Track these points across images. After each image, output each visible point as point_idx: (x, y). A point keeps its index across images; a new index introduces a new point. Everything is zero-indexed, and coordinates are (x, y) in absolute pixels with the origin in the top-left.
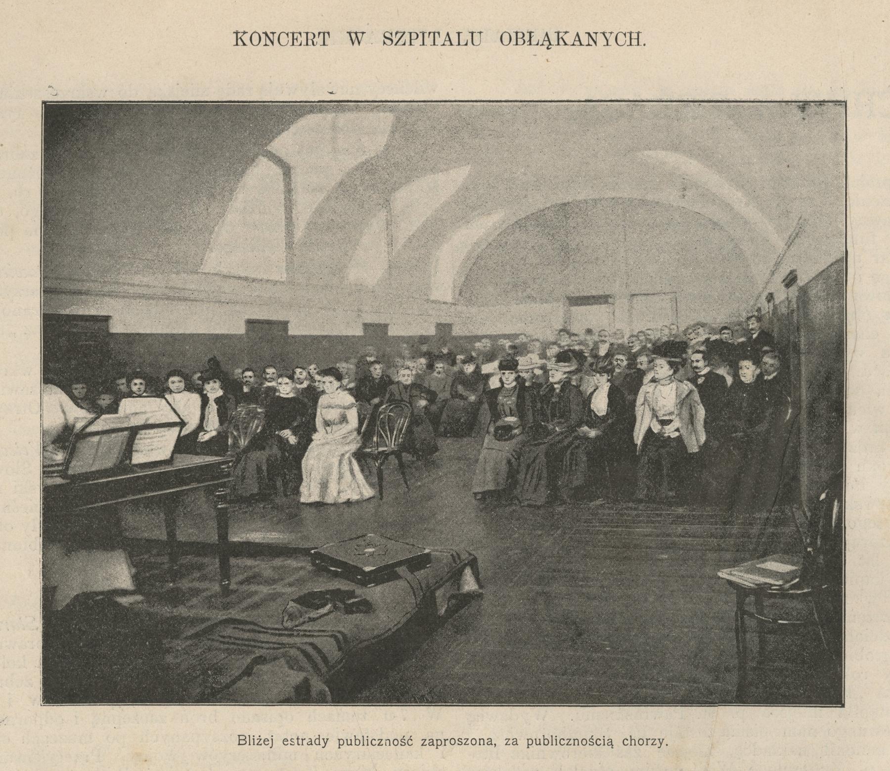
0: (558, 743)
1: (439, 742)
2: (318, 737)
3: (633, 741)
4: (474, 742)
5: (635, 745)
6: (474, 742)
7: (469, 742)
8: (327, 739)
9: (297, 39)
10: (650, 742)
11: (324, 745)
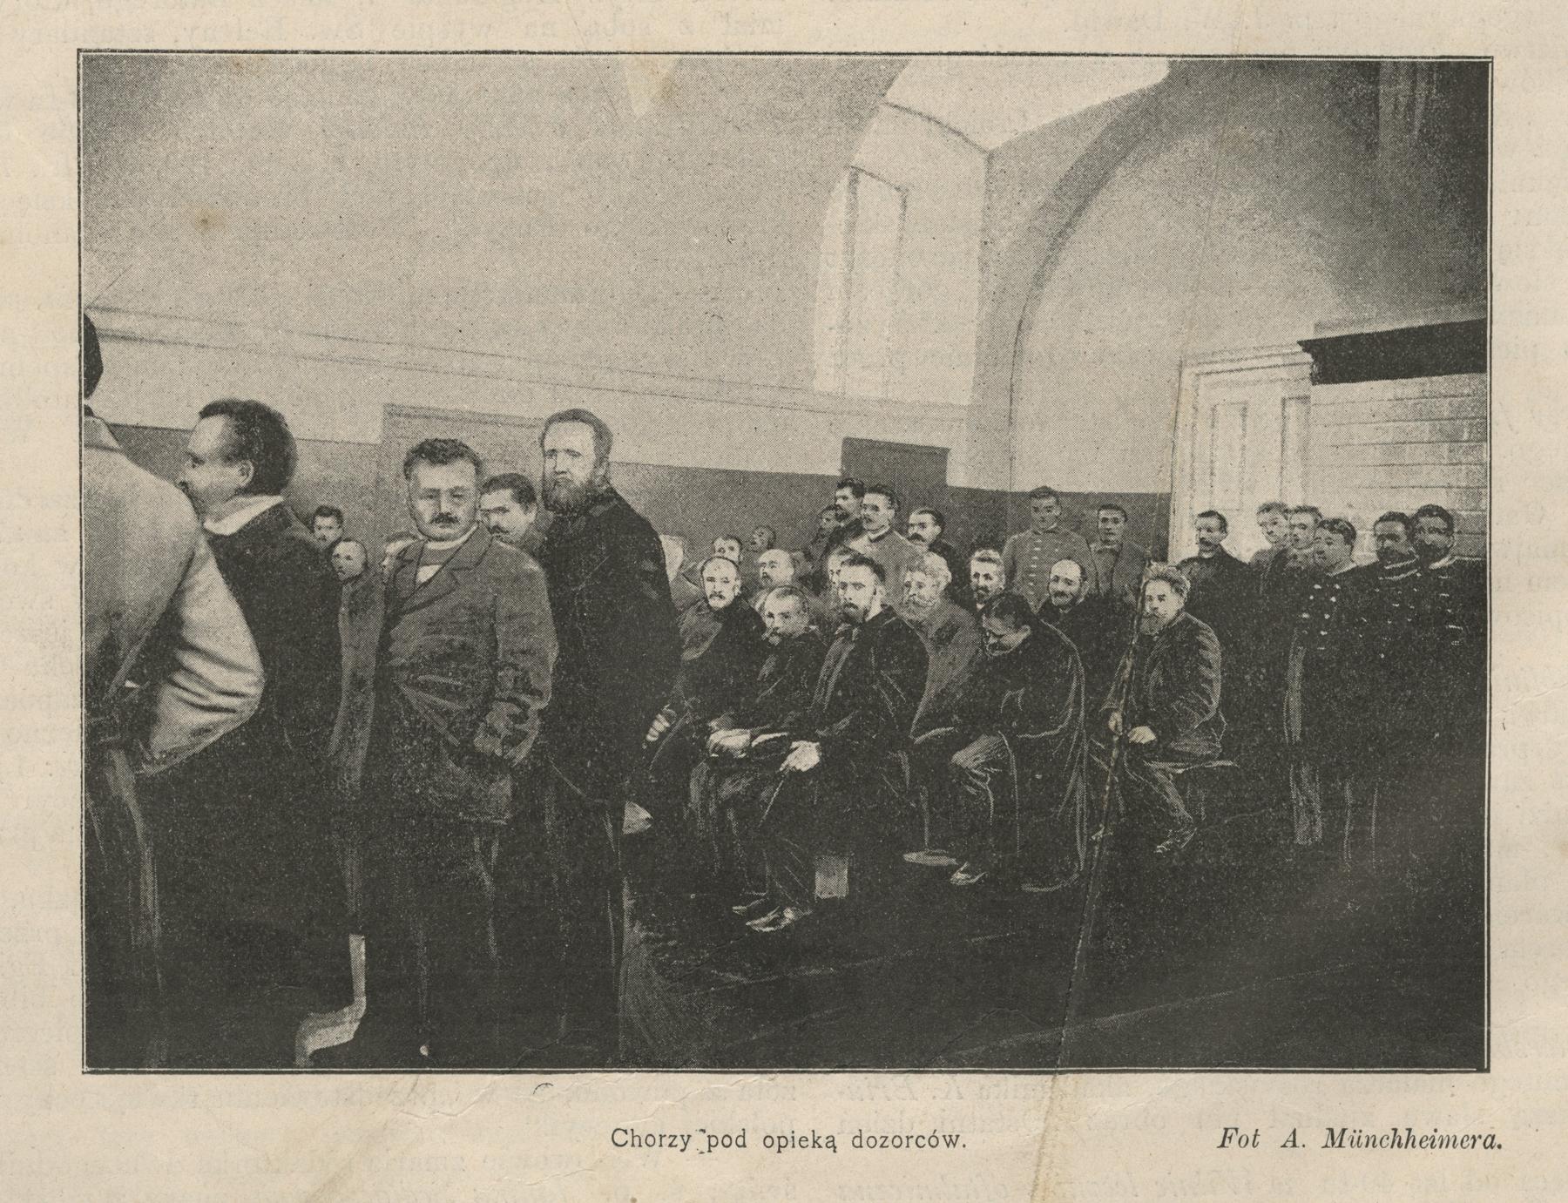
0: (643, 1144)
1: (783, 1140)
2: (742, 1134)
3: (636, 1139)
4: (897, 1142)
5: (640, 1146)
6: (897, 1142)
7: (880, 1142)
8: (689, 1136)
9: (1230, 1138)
10: (666, 1141)
11: (683, 1147)
